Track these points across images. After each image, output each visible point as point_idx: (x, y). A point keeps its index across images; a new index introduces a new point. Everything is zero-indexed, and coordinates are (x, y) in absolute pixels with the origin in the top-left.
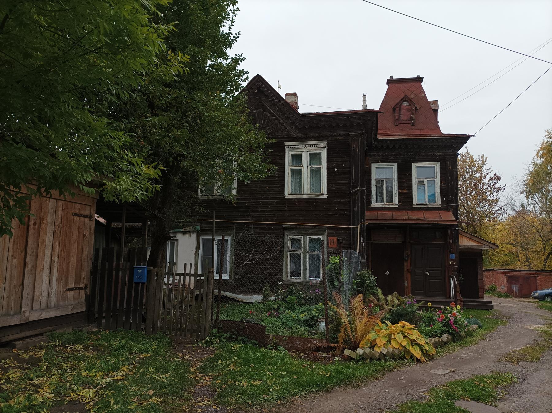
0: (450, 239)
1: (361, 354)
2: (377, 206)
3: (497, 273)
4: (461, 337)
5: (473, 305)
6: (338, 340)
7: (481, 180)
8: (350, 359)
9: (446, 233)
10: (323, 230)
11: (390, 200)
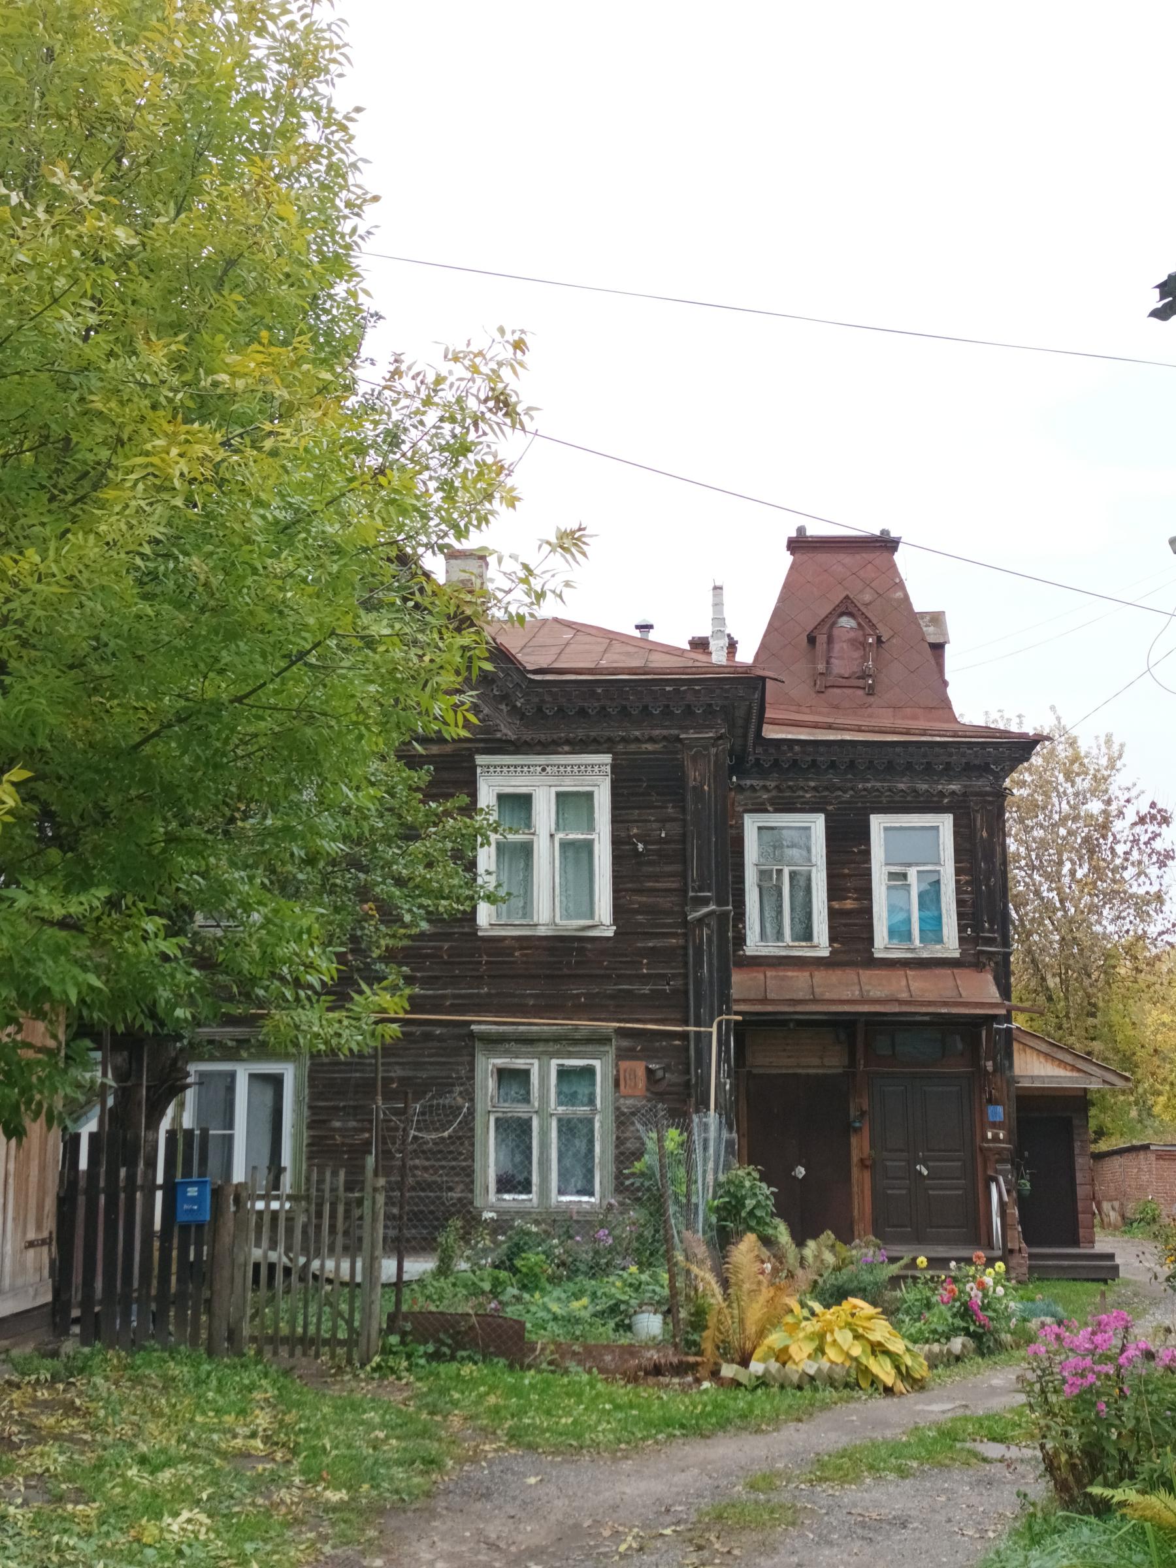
0: (987, 1060)
2: (764, 952)
3: (1160, 1156)
4: (1001, 1346)
6: (694, 1350)
9: (974, 1039)
10: (604, 1040)
11: (806, 934)
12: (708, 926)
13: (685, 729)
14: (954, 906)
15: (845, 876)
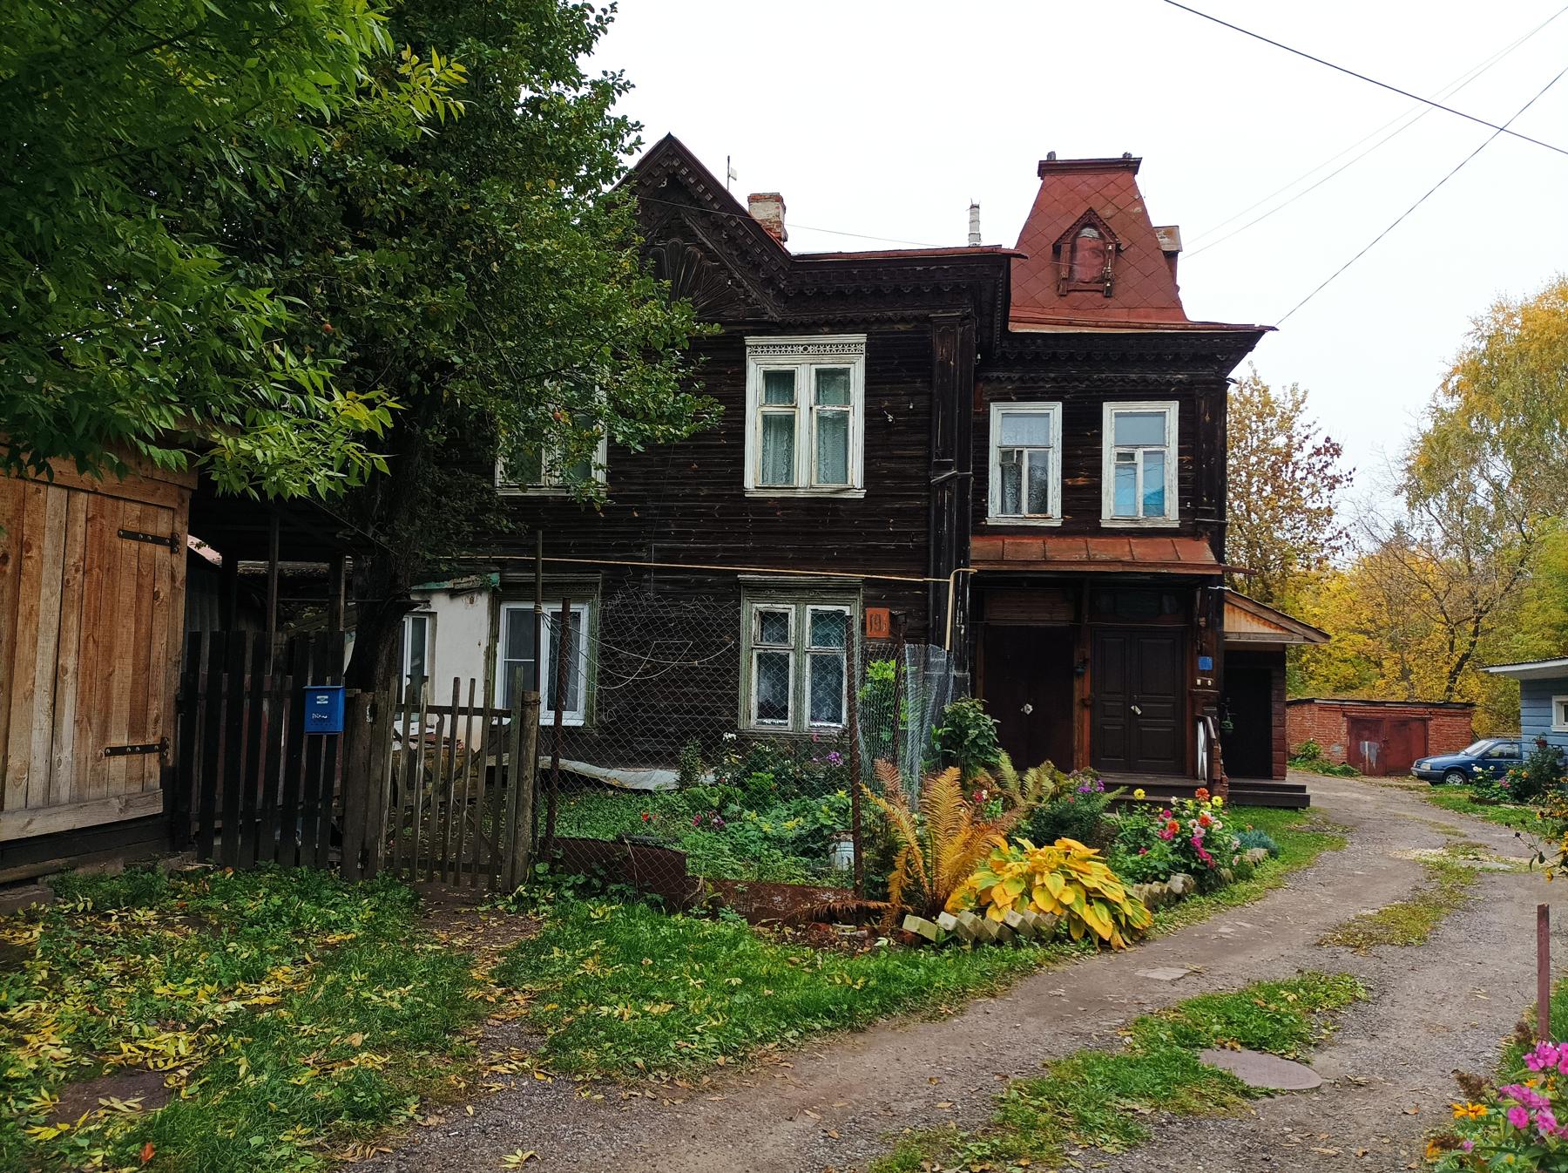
3: (1322, 708)
4: (1221, 882)
6: (887, 893)
8: (920, 941)
9: (1196, 597)
11: (1041, 506)
12: (949, 489)
13: (934, 309)
14: (1176, 482)
15: (1077, 456)
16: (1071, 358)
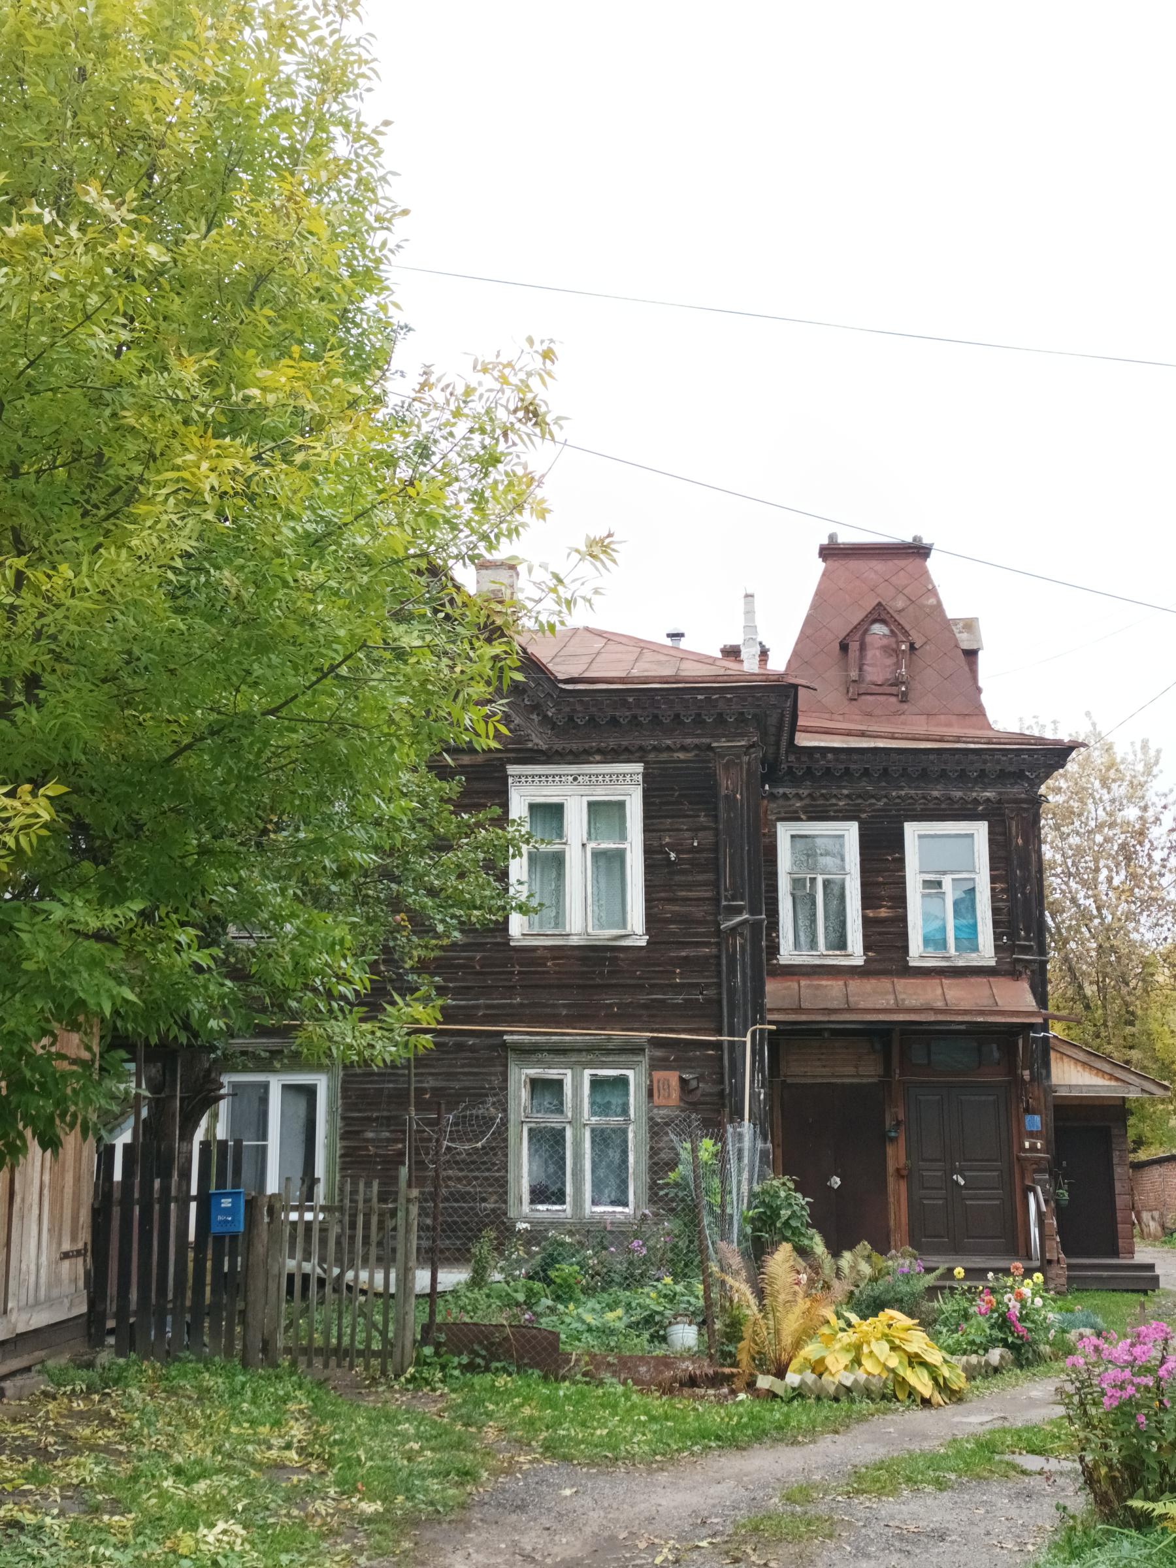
0: (1024, 1069)
1: (796, 1385)
2: (798, 961)
4: (1039, 1358)
5: (1100, 1278)
6: (731, 1362)
7: (1142, 833)
9: (1011, 1049)
10: (637, 1050)
11: (840, 943)
12: (741, 935)
13: (716, 737)
15: (878, 884)
16: (866, 772)
